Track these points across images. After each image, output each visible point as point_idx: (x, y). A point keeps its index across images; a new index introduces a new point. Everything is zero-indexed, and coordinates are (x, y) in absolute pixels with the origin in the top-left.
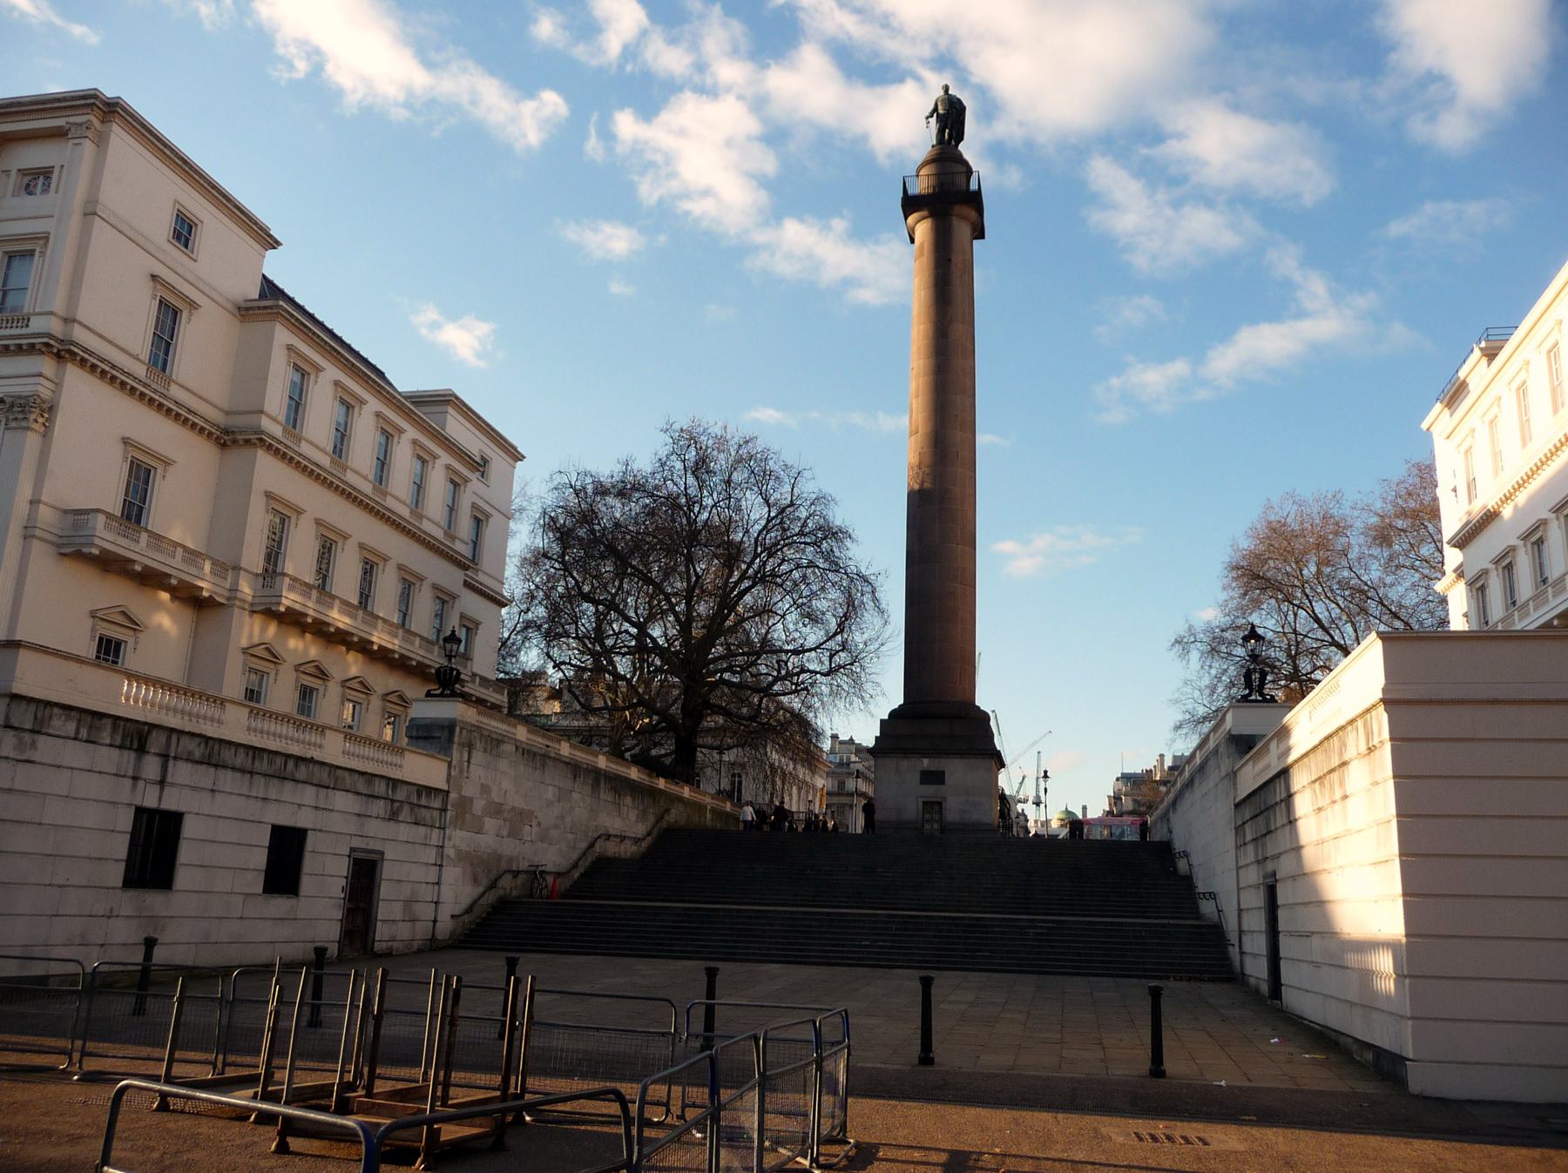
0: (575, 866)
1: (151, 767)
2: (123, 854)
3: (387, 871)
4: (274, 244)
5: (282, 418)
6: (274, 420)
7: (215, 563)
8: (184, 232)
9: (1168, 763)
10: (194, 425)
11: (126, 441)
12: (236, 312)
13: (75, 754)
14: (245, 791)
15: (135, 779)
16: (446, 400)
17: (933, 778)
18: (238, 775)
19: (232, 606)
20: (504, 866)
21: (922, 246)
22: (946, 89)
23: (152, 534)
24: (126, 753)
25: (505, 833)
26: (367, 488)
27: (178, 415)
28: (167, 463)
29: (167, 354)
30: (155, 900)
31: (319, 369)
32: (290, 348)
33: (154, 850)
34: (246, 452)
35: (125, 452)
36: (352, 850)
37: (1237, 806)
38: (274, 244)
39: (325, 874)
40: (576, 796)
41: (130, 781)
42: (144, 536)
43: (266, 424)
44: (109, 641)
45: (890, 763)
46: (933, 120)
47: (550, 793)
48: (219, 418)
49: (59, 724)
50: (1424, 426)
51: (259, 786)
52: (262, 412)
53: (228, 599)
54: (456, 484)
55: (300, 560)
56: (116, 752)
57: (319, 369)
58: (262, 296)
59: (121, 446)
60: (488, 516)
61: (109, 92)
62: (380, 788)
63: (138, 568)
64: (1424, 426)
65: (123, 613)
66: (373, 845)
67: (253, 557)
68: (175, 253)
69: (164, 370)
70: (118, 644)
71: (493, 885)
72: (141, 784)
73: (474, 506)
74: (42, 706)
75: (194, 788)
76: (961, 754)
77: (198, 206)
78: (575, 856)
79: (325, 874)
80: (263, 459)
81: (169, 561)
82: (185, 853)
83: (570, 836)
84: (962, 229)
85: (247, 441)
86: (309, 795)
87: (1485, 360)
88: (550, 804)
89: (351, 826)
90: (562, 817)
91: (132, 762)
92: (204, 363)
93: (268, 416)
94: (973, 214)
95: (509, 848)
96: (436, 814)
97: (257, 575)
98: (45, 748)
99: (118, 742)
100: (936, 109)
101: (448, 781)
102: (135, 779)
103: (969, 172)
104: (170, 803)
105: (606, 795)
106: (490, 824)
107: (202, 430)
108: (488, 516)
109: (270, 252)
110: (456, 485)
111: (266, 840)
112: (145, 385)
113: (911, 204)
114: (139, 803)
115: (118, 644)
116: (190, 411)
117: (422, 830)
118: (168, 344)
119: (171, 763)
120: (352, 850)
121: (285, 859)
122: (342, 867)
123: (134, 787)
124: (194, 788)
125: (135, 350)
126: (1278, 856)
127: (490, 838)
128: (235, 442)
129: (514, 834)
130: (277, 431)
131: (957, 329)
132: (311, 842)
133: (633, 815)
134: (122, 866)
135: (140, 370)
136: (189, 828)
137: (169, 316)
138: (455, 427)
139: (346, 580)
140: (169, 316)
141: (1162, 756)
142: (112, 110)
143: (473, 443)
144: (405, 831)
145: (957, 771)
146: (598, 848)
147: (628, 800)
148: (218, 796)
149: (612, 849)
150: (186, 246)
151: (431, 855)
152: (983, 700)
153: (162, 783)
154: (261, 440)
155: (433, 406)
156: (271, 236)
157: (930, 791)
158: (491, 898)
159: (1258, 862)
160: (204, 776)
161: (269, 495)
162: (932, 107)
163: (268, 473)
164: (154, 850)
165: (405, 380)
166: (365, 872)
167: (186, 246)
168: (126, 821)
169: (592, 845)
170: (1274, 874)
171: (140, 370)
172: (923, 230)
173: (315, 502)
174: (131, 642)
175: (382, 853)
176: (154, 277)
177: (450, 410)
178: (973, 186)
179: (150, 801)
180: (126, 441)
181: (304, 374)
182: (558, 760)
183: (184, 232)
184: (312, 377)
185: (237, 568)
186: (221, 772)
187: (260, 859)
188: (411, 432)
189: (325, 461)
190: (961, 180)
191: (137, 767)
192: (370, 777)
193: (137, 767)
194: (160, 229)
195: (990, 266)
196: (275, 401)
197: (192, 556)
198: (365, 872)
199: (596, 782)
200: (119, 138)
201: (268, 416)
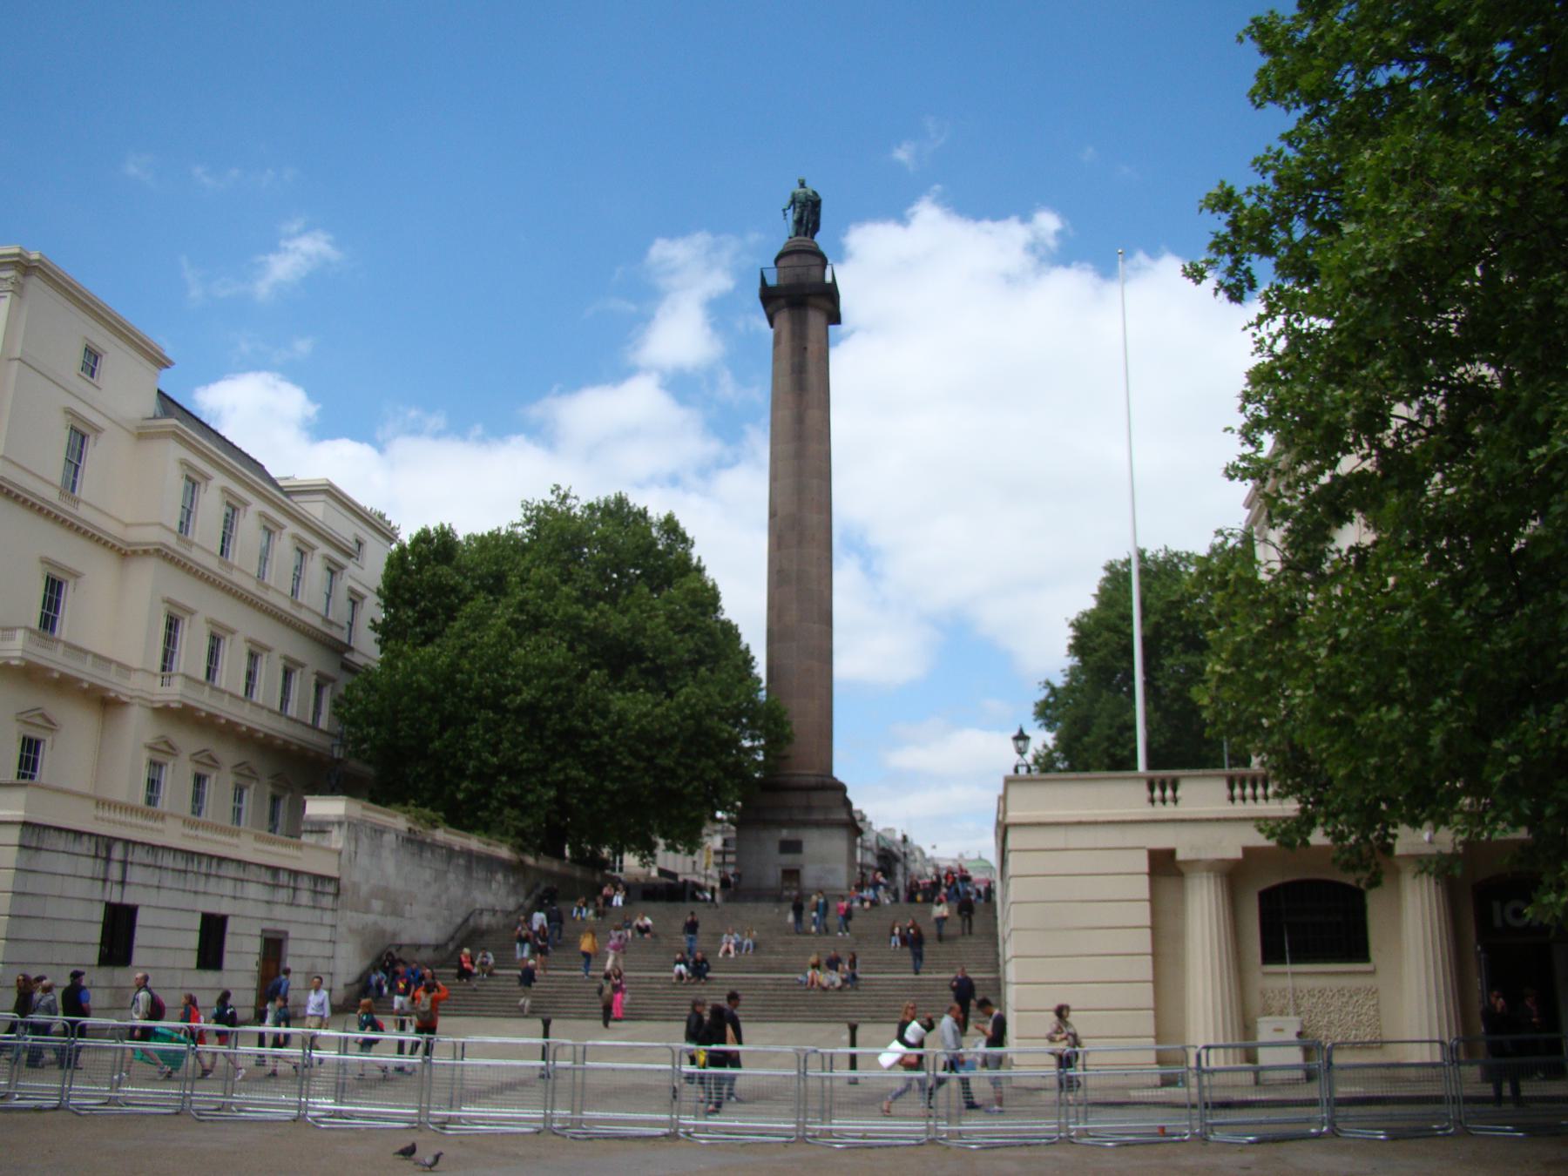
0: (452, 938)
1: (115, 872)
2: (98, 939)
3: (291, 948)
13: (62, 864)
14: (181, 886)
15: (105, 880)
17: (793, 847)
23: (68, 645)
28: (76, 575)
29: (76, 475)
33: (118, 932)
36: (263, 931)
39: (243, 953)
40: (451, 876)
41: (100, 883)
44: (30, 740)
46: (790, 212)
47: (427, 875)
49: (61, 843)
51: (191, 882)
54: (334, 570)
62: (284, 878)
66: (281, 927)
68: (82, 385)
69: (73, 490)
70: (38, 743)
73: (352, 591)
75: (145, 886)
76: (818, 825)
77: (102, 339)
78: (451, 929)
79: (243, 953)
82: (140, 937)
86: (228, 887)
88: (427, 884)
89: (261, 911)
90: (439, 897)
94: (829, 306)
95: (390, 924)
96: (330, 898)
102: (105, 880)
104: (129, 899)
105: (480, 874)
106: (377, 905)
109: (165, 371)
110: (332, 573)
111: (198, 926)
114: (107, 898)
115: (38, 743)
117: (318, 912)
118: (77, 467)
120: (263, 931)
121: (212, 940)
122: (256, 945)
124: (145, 886)
127: (376, 917)
131: (813, 415)
132: (231, 926)
133: (503, 891)
134: (195, 955)
136: (142, 918)
137: (79, 438)
139: (232, 672)
140: (79, 438)
143: (347, 529)
146: (472, 922)
147: (500, 877)
149: (486, 920)
150: (92, 375)
152: (840, 772)
153: (123, 883)
157: (788, 860)
160: (151, 877)
162: (788, 199)
164: (118, 932)
166: (273, 947)
168: (98, 913)
169: (466, 920)
173: (208, 607)
174: (49, 740)
175: (286, 933)
179: (116, 899)
181: (194, 484)
182: (434, 846)
183: (92, 360)
186: (164, 873)
187: (193, 940)
191: (106, 871)
192: (275, 870)
198: (273, 947)
199: (470, 862)
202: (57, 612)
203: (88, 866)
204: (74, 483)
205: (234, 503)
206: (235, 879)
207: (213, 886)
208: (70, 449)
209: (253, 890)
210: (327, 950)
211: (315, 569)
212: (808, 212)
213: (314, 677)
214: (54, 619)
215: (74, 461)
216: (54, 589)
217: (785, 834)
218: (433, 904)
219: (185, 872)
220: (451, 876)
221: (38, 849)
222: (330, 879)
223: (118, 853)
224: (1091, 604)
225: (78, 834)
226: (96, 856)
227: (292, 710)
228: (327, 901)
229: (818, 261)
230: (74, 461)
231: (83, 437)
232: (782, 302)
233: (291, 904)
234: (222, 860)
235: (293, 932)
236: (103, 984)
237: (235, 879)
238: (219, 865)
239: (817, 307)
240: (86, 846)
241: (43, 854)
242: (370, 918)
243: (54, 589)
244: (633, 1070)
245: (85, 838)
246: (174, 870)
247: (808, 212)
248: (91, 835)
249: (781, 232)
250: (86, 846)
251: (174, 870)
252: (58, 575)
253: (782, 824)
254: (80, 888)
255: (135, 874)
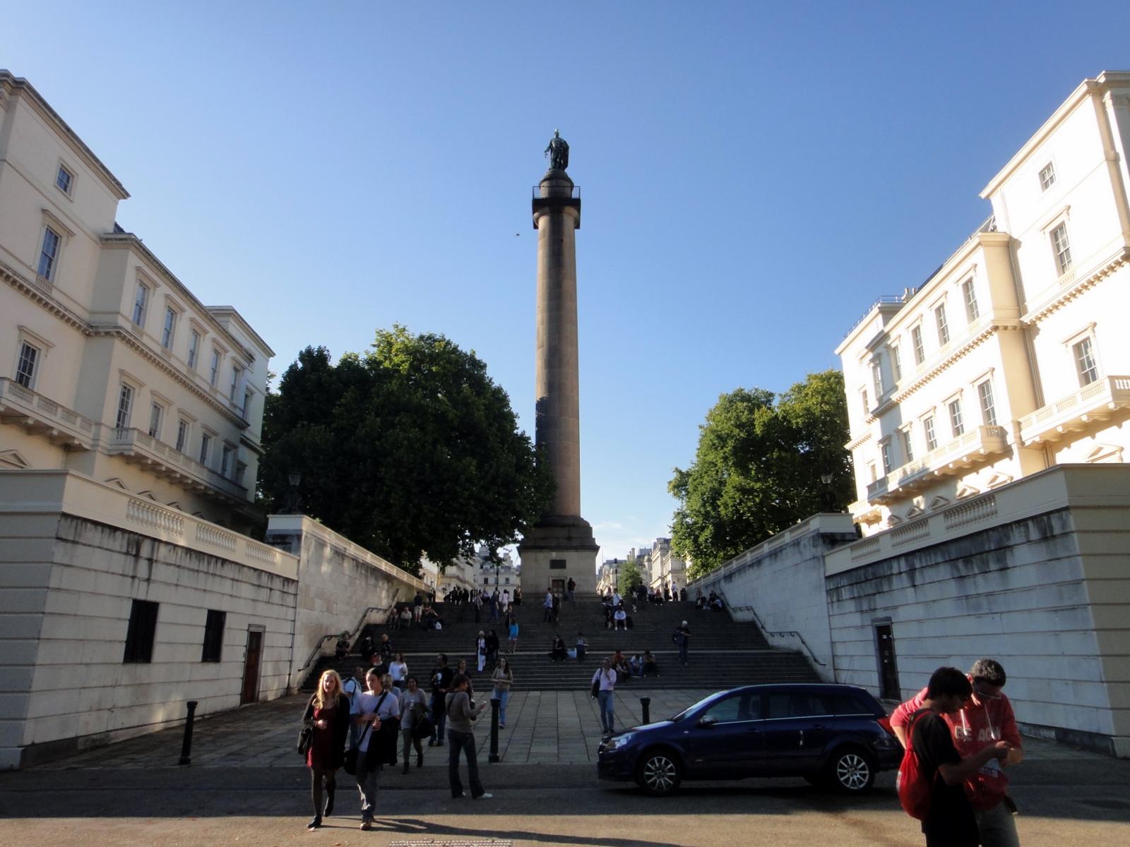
3: (897, 632)
4: (125, 195)
5: (131, 318)
6: (126, 319)
7: (84, 419)
8: (65, 180)
9: (637, 553)
10: (69, 320)
11: (21, 329)
12: (98, 241)
13: (98, 559)
14: (194, 586)
15: (133, 577)
16: (230, 313)
18: (191, 573)
19: (95, 451)
20: (324, 633)
21: (544, 230)
22: (557, 135)
24: (129, 557)
25: (325, 610)
26: (184, 370)
27: (58, 312)
28: (49, 346)
29: (49, 266)
30: (140, 670)
31: (156, 285)
32: (138, 269)
34: (107, 340)
35: (20, 335)
37: (827, 578)
38: (125, 195)
41: (130, 580)
42: (36, 399)
43: (121, 322)
45: (531, 555)
46: (549, 153)
48: (86, 316)
49: (93, 535)
50: (837, 352)
51: (201, 581)
52: (118, 313)
53: (92, 446)
55: (140, 417)
56: (123, 557)
57: (156, 285)
58: (115, 232)
59: (17, 332)
60: (252, 393)
61: (16, 74)
63: (30, 422)
64: (837, 352)
65: (15, 455)
67: (110, 416)
68: (58, 196)
69: (47, 277)
71: (319, 647)
72: (137, 581)
74: (80, 522)
76: (576, 549)
80: (119, 345)
81: (53, 417)
83: (354, 609)
84: (568, 222)
85: (107, 333)
86: (227, 586)
87: (880, 317)
91: (132, 564)
92: (76, 276)
93: (123, 316)
97: (113, 429)
98: (82, 555)
99: (124, 550)
100: (550, 147)
101: (298, 574)
103: (572, 186)
104: (152, 598)
105: (372, 581)
106: (318, 603)
107: (74, 324)
108: (252, 393)
111: (204, 621)
112: (37, 289)
113: (538, 205)
114: (134, 596)
116: (66, 309)
118: (51, 260)
119: (154, 564)
123: (133, 582)
125: (29, 262)
126: (895, 608)
128: (97, 333)
129: (329, 610)
130: (128, 326)
131: (567, 284)
134: (124, 646)
135: (32, 277)
137: (53, 240)
138: (233, 329)
139: (169, 433)
140: (53, 240)
141: (633, 549)
142: (20, 86)
144: (276, 611)
145: (571, 557)
148: (180, 589)
150: (65, 190)
151: (287, 627)
152: (585, 514)
154: (118, 333)
155: (220, 318)
156: (123, 189)
157: (557, 573)
158: (316, 657)
159: (862, 612)
161: (122, 372)
163: (121, 355)
165: (207, 301)
167: (65, 190)
168: (126, 611)
170: (889, 619)
171: (32, 277)
172: (543, 222)
173: (152, 381)
175: (265, 627)
176: (44, 211)
177: (231, 320)
178: (575, 195)
180: (21, 329)
183: (65, 180)
184: (151, 291)
185: (99, 424)
186: (182, 571)
187: (199, 635)
188: (212, 334)
189: (158, 350)
190: (568, 190)
191: (135, 569)
193: (135, 569)
194: (49, 179)
195: (586, 243)
196: (127, 308)
197: (70, 414)
198: (255, 641)
200: (22, 105)
201: (123, 316)
202: (30, 373)
203: (121, 563)
204: (48, 272)
205: (174, 307)
206: (233, 579)
207: (213, 584)
208: (46, 245)
209: (246, 591)
210: (837, 636)
211: (226, 366)
212: (560, 152)
213: (223, 444)
214: (28, 379)
215: (49, 258)
216: (29, 356)
217: (554, 555)
218: (348, 604)
219: (198, 571)
220: (358, 582)
221: (74, 542)
222: (293, 581)
223: (145, 550)
224: (1035, 341)
225: (115, 529)
226: (127, 553)
227: (209, 463)
228: (290, 600)
229: (569, 185)
230: (49, 258)
231: (56, 238)
232: (547, 209)
233: (268, 602)
234: (224, 561)
235: (270, 626)
236: (124, 682)
237: (233, 579)
238: (222, 564)
239: (570, 214)
240: (119, 543)
241: (80, 547)
242: (316, 613)
243: (29, 356)
244: (520, 655)
245: (118, 533)
246: (189, 569)
247: (560, 152)
248: (124, 531)
249: (545, 165)
250: (119, 543)
251: (189, 569)
252: (34, 343)
253: (552, 549)
254: (110, 585)
255: (160, 572)
